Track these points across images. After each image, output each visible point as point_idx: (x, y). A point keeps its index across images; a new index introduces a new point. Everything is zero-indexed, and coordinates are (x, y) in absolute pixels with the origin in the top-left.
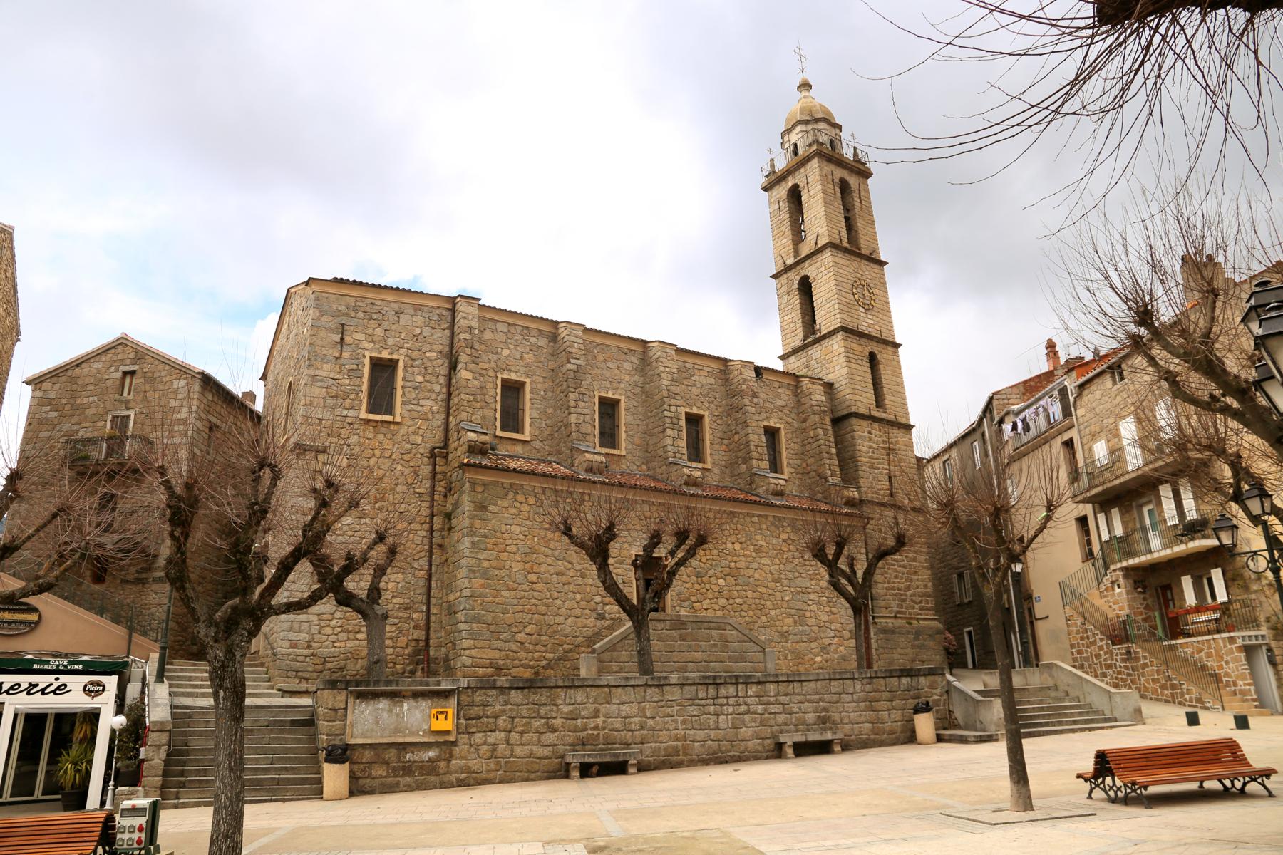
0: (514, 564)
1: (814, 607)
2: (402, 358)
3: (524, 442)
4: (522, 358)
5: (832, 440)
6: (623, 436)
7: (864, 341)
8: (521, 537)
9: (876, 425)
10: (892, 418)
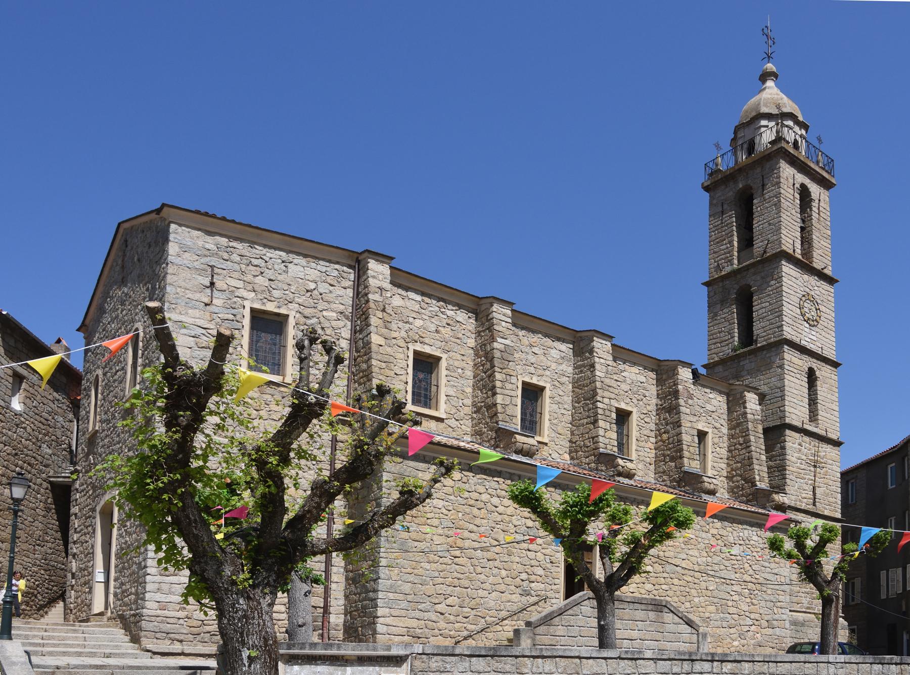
0: (435, 538)
1: (736, 598)
2: (292, 314)
3: (439, 420)
4: (437, 331)
5: (763, 447)
6: (546, 424)
7: (806, 358)
8: (444, 511)
9: (807, 439)
10: (823, 433)
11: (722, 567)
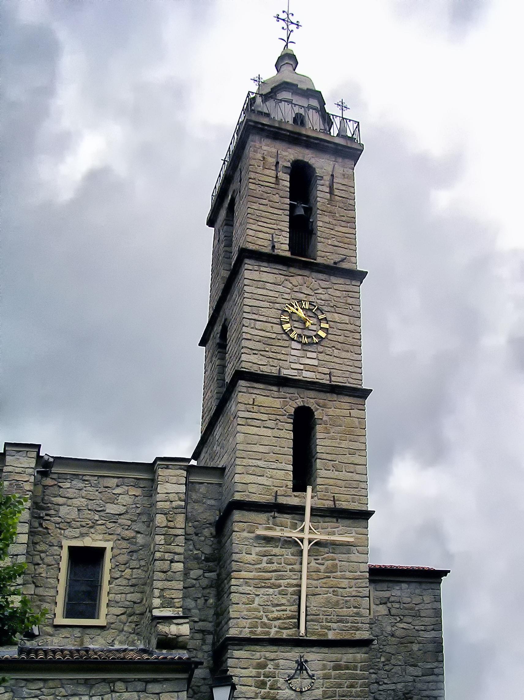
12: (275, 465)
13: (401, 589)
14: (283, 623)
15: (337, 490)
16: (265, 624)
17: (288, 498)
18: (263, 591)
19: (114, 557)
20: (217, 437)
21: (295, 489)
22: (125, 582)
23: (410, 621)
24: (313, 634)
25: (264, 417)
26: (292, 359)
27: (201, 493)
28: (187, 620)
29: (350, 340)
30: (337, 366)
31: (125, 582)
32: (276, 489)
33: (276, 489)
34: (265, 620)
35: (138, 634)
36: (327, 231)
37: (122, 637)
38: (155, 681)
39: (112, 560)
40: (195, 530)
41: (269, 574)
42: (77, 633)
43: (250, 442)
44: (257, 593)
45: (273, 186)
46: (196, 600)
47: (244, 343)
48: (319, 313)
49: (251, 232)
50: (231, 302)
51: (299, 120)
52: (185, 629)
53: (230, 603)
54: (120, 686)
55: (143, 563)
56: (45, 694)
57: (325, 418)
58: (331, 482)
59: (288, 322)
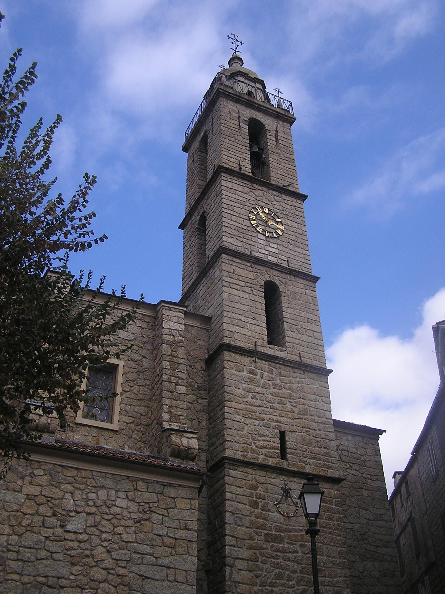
9: (264, 365)
11: (43, 553)
12: (253, 321)
13: (347, 440)
14: (268, 452)
15: (301, 349)
16: (254, 450)
17: (265, 349)
18: (250, 421)
19: (125, 373)
20: (201, 294)
21: (269, 343)
22: (133, 396)
23: (358, 469)
24: (293, 465)
25: (243, 284)
26: (259, 246)
27: (193, 334)
28: (195, 436)
29: (300, 240)
30: (292, 256)
31: (133, 396)
32: (255, 340)
33: (255, 340)
34: (253, 446)
35: (143, 442)
36: (277, 165)
37: (131, 443)
38: (171, 485)
39: (124, 376)
40: (189, 363)
41: (254, 408)
42: (94, 432)
43: (233, 300)
44: (246, 422)
45: (237, 130)
46: (192, 421)
47: (224, 229)
48: (276, 217)
49: (224, 156)
50: (209, 201)
51: (249, 93)
52: (194, 443)
53: (225, 427)
54: (141, 485)
55: (148, 382)
56: (78, 482)
57: (287, 292)
58: (297, 341)
59: (255, 220)
